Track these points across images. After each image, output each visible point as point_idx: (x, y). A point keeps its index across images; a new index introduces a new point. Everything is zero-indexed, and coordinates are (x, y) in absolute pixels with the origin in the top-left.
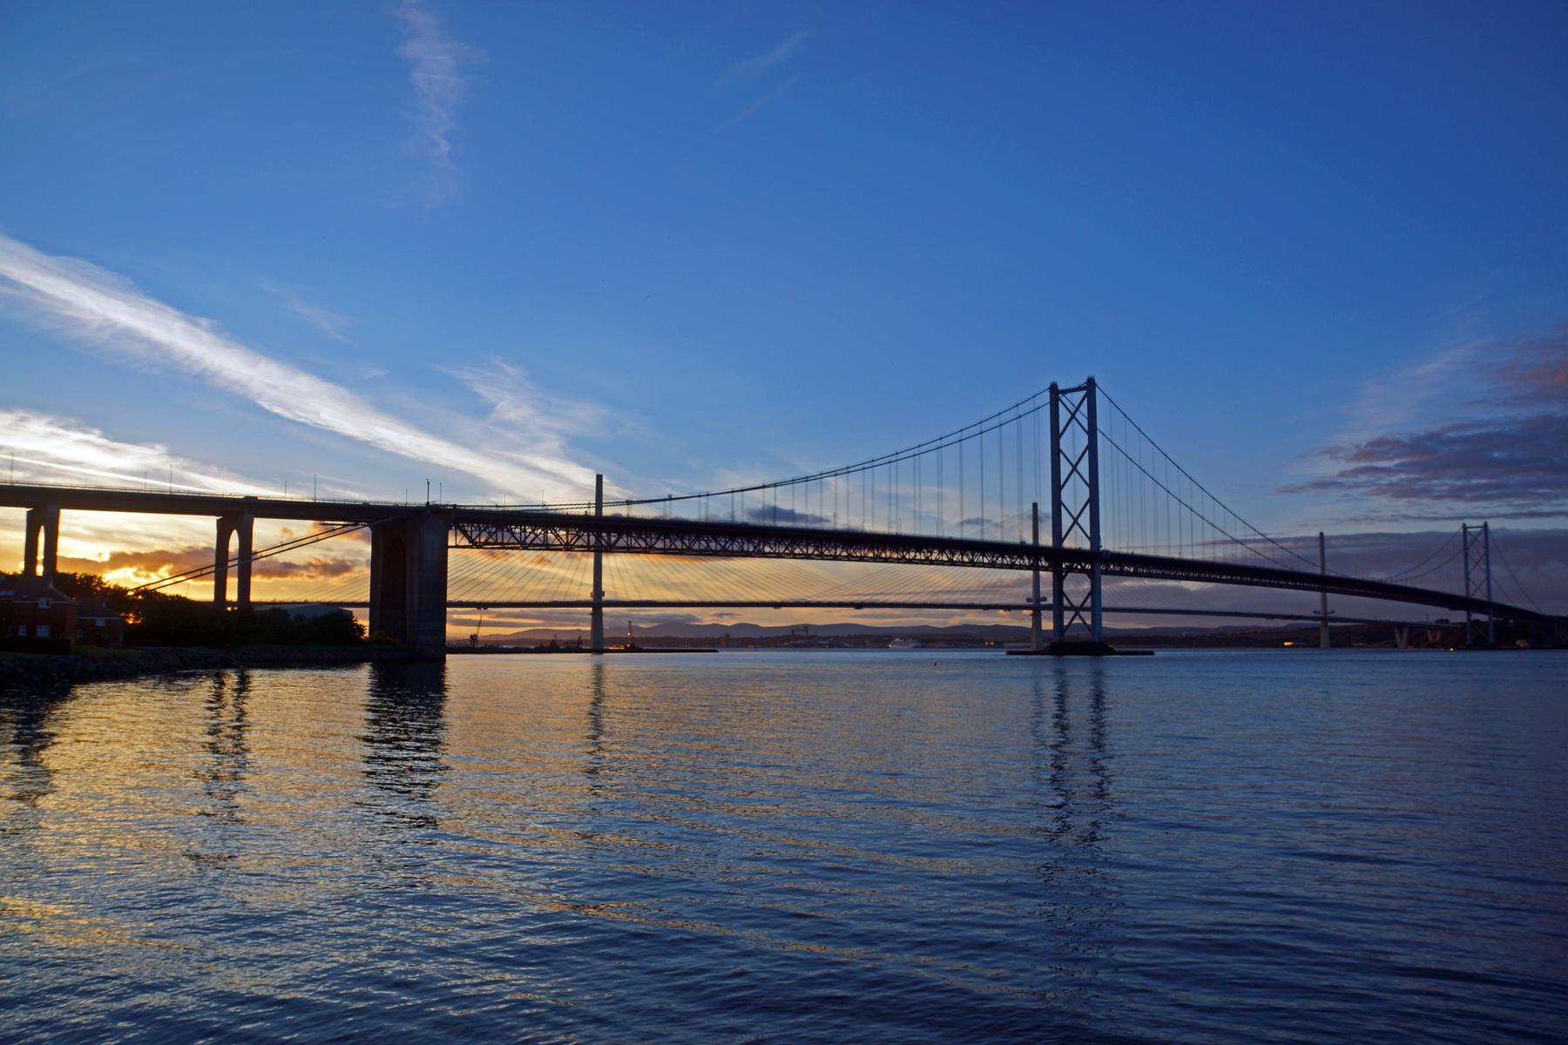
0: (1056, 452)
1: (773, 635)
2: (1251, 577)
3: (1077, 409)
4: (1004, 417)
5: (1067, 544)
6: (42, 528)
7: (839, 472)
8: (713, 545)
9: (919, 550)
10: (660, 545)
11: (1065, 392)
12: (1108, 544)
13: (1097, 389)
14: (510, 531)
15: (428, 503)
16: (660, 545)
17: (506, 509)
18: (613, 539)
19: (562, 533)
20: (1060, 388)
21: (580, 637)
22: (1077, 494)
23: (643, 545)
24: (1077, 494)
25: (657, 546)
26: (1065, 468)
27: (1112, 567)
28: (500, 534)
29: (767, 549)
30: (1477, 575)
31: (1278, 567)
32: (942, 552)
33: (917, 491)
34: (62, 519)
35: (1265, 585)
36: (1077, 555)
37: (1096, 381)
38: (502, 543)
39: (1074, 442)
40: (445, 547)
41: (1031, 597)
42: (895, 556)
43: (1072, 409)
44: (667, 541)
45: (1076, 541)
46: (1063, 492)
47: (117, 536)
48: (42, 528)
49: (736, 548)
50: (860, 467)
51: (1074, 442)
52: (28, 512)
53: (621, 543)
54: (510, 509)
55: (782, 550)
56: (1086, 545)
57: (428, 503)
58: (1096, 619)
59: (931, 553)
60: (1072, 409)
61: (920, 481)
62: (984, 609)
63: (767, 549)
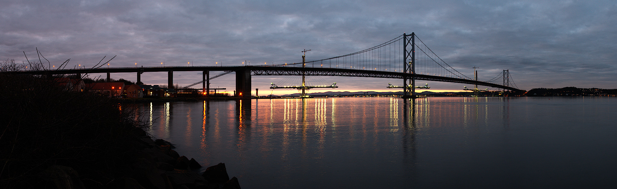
3: (410, 39)
7: (361, 52)
9: (354, 73)
11: (407, 36)
21: (142, 66)
22: (506, 81)
23: (317, 74)
24: (506, 81)
26: (407, 54)
27: (384, 76)
28: (285, 72)
30: (425, 73)
33: (385, 59)
35: (432, 80)
38: (286, 74)
50: (366, 51)
53: (311, 74)
58: (255, 98)
59: (393, 76)
60: (409, 40)
62: (493, 87)
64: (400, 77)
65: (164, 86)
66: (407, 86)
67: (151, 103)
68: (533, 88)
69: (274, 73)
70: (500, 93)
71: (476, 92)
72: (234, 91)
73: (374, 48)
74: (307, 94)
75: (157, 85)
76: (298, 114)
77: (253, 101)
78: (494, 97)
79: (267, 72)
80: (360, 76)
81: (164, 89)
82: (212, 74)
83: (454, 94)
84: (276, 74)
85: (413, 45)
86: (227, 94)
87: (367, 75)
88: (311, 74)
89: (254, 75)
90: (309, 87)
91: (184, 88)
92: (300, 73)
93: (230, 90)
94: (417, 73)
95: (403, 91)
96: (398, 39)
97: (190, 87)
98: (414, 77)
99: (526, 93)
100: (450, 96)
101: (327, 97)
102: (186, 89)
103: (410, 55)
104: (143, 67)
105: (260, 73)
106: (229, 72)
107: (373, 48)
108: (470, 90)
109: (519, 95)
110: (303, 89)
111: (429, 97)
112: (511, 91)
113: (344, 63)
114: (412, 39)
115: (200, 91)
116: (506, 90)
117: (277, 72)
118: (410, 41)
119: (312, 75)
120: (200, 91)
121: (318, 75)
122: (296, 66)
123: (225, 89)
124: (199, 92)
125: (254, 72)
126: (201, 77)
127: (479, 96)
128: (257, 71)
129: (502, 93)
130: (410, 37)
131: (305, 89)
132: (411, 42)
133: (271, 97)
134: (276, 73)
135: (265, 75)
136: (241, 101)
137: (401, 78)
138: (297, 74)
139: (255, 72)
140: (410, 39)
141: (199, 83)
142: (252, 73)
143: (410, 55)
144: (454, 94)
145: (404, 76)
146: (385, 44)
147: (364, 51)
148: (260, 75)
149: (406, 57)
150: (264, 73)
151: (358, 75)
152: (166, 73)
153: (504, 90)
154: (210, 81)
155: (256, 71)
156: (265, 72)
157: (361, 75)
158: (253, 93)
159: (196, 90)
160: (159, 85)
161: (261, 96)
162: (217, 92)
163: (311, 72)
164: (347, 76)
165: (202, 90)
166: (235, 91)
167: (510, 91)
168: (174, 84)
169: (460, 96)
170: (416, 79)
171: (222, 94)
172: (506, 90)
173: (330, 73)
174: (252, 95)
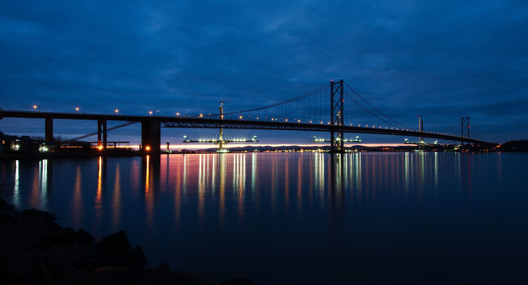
3: (338, 88)
6: (100, 158)
8: (260, 127)
10: (239, 126)
14: (213, 124)
15: (154, 116)
16: (239, 126)
18: (228, 125)
21: (2, 109)
23: (235, 127)
25: (238, 127)
29: (273, 128)
32: (315, 128)
35: (413, 136)
40: (160, 127)
44: (250, 126)
47: (197, 152)
48: (100, 158)
49: (266, 128)
52: (46, 120)
57: (154, 116)
60: (337, 88)
63: (273, 128)
64: (327, 130)
65: (39, 138)
66: (335, 140)
67: (17, 162)
68: (513, 140)
69: (188, 125)
70: (456, 147)
71: (421, 146)
72: (140, 146)
74: (224, 149)
75: (27, 135)
77: (163, 156)
78: (448, 152)
79: (180, 124)
81: (40, 142)
82: (110, 124)
83: (392, 149)
84: (190, 126)
86: (130, 148)
87: (290, 128)
88: (230, 126)
89: (165, 127)
90: (227, 141)
91: (71, 140)
92: (216, 125)
93: (135, 143)
94: (346, 125)
95: (330, 145)
97: (80, 140)
98: (343, 130)
99: (497, 147)
100: (386, 151)
101: (246, 151)
102: (73, 142)
104: (3, 109)
106: (134, 122)
107: (297, 99)
108: (413, 143)
110: (220, 143)
111: (360, 152)
112: (472, 144)
114: (340, 87)
115: (94, 144)
116: (465, 143)
117: (191, 124)
119: (230, 128)
120: (94, 144)
123: (128, 142)
124: (93, 146)
125: (165, 124)
126: (96, 127)
127: (425, 151)
128: (168, 122)
129: (458, 147)
131: (223, 143)
133: (184, 152)
134: (190, 125)
135: (178, 127)
137: (328, 131)
138: (214, 126)
139: (166, 124)
140: (338, 88)
141: (92, 134)
142: (163, 125)
144: (392, 149)
146: (309, 94)
147: (286, 102)
148: (171, 127)
149: (334, 107)
150: (176, 124)
151: (280, 128)
152: (43, 121)
153: (462, 143)
154: (108, 133)
155: (167, 123)
156: (178, 123)
157: (283, 128)
158: (163, 147)
159: (89, 144)
160: (31, 135)
161: (172, 151)
162: (117, 147)
163: (229, 125)
164: (269, 129)
165: (97, 144)
166: (141, 144)
167: (471, 144)
168: (55, 135)
169: (400, 151)
170: (345, 132)
171: (125, 148)
172: (465, 143)
173: (250, 126)
174: (161, 149)
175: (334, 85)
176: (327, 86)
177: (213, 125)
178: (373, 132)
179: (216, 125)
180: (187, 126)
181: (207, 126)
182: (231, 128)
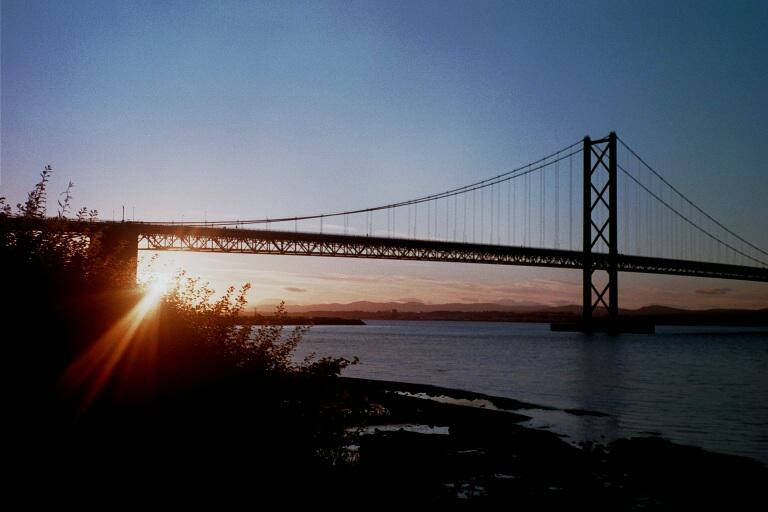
0: (588, 185)
1: (430, 310)
2: (677, 269)
3: (604, 153)
4: (562, 155)
5: (594, 250)
8: (397, 253)
9: (438, 251)
10: (341, 251)
12: (621, 250)
13: (618, 142)
14: (274, 243)
17: (240, 227)
18: (311, 247)
19: (279, 244)
20: (592, 139)
27: (476, 256)
31: (753, 264)
32: (543, 258)
34: (624, 253)
36: (600, 257)
37: (618, 135)
39: (600, 178)
41: (40, 210)
42: (528, 261)
43: (600, 154)
45: (600, 248)
46: (593, 213)
50: (489, 182)
51: (600, 178)
53: (316, 250)
54: (741, 455)
55: (440, 255)
56: (606, 250)
60: (600, 154)
61: (394, 228)
73: (497, 180)
76: (432, 427)
80: (455, 260)
85: (612, 170)
87: (476, 256)
89: (149, 249)
96: (568, 152)
103: (603, 200)
105: (167, 244)
109: (45, 251)
113: (597, 213)
114: (608, 153)
118: (602, 156)
121: (334, 254)
122: (247, 227)
130: (603, 146)
132: (606, 160)
136: (443, 430)
137: (576, 267)
140: (604, 153)
143: (603, 200)
145: (585, 260)
146: (527, 169)
150: (210, 244)
151: (449, 257)
156: (182, 240)
157: (458, 256)
164: (418, 259)
175: (593, 146)
176: (574, 149)
177: (272, 247)
178: (440, 255)
179: (280, 247)
180: (206, 248)
181: (257, 248)
182: (321, 254)
